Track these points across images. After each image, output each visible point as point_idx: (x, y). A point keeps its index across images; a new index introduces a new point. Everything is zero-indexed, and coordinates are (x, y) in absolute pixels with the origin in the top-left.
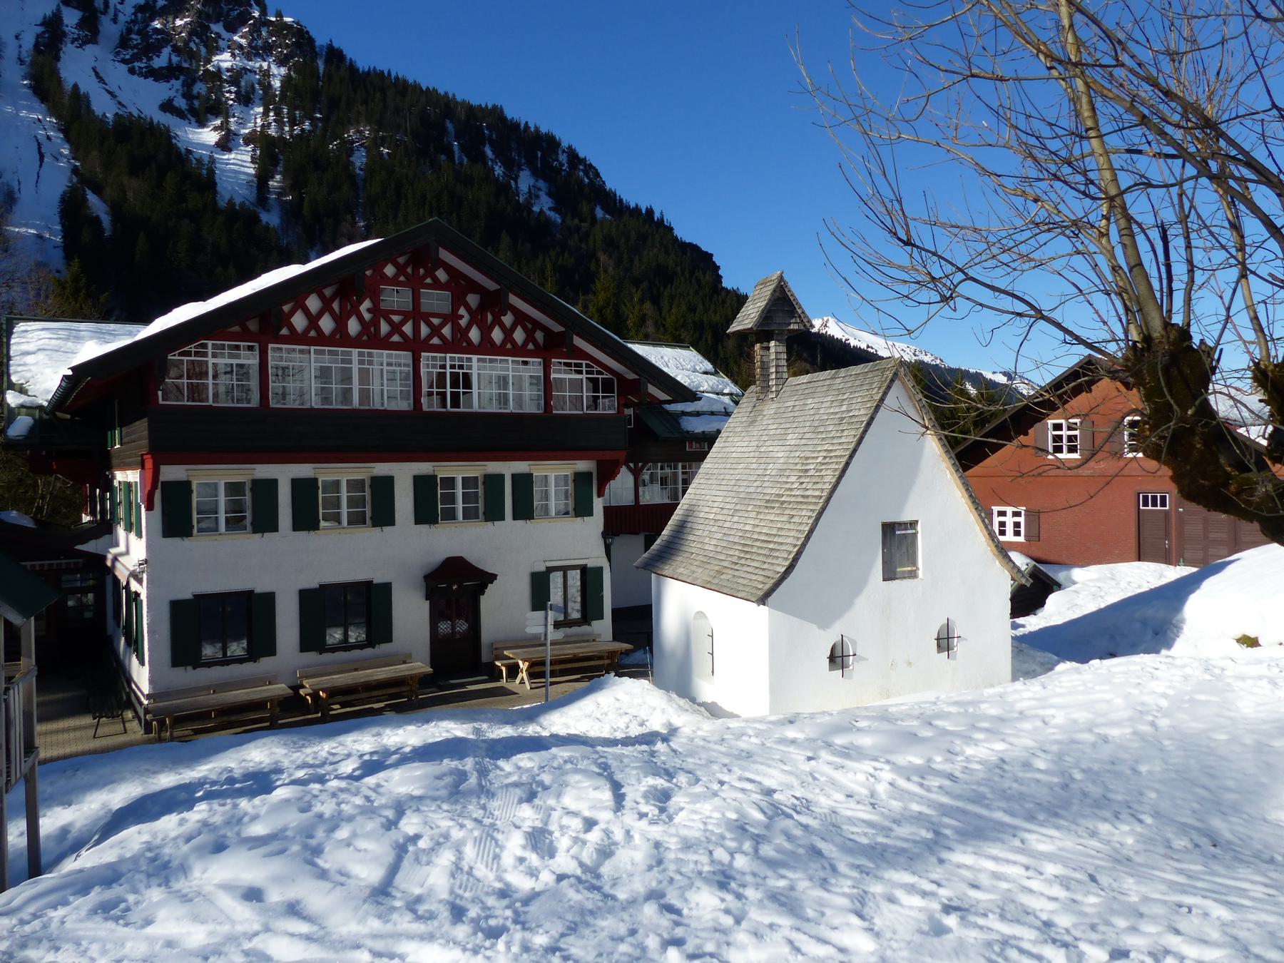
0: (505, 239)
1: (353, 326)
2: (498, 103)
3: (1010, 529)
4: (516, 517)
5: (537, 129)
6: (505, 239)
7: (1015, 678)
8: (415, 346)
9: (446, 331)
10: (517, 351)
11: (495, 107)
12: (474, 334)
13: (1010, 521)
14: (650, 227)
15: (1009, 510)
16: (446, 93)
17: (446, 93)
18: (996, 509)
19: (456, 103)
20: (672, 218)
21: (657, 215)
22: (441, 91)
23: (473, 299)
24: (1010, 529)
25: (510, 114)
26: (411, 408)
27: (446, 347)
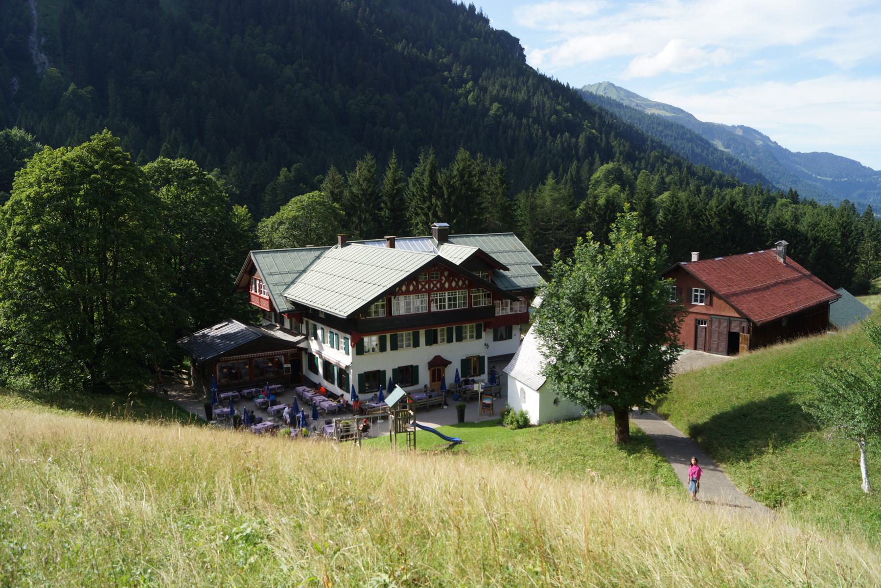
1: (411, 288)
4: (457, 341)
8: (429, 292)
9: (438, 285)
12: (447, 285)
21: (477, 11)
23: (446, 273)
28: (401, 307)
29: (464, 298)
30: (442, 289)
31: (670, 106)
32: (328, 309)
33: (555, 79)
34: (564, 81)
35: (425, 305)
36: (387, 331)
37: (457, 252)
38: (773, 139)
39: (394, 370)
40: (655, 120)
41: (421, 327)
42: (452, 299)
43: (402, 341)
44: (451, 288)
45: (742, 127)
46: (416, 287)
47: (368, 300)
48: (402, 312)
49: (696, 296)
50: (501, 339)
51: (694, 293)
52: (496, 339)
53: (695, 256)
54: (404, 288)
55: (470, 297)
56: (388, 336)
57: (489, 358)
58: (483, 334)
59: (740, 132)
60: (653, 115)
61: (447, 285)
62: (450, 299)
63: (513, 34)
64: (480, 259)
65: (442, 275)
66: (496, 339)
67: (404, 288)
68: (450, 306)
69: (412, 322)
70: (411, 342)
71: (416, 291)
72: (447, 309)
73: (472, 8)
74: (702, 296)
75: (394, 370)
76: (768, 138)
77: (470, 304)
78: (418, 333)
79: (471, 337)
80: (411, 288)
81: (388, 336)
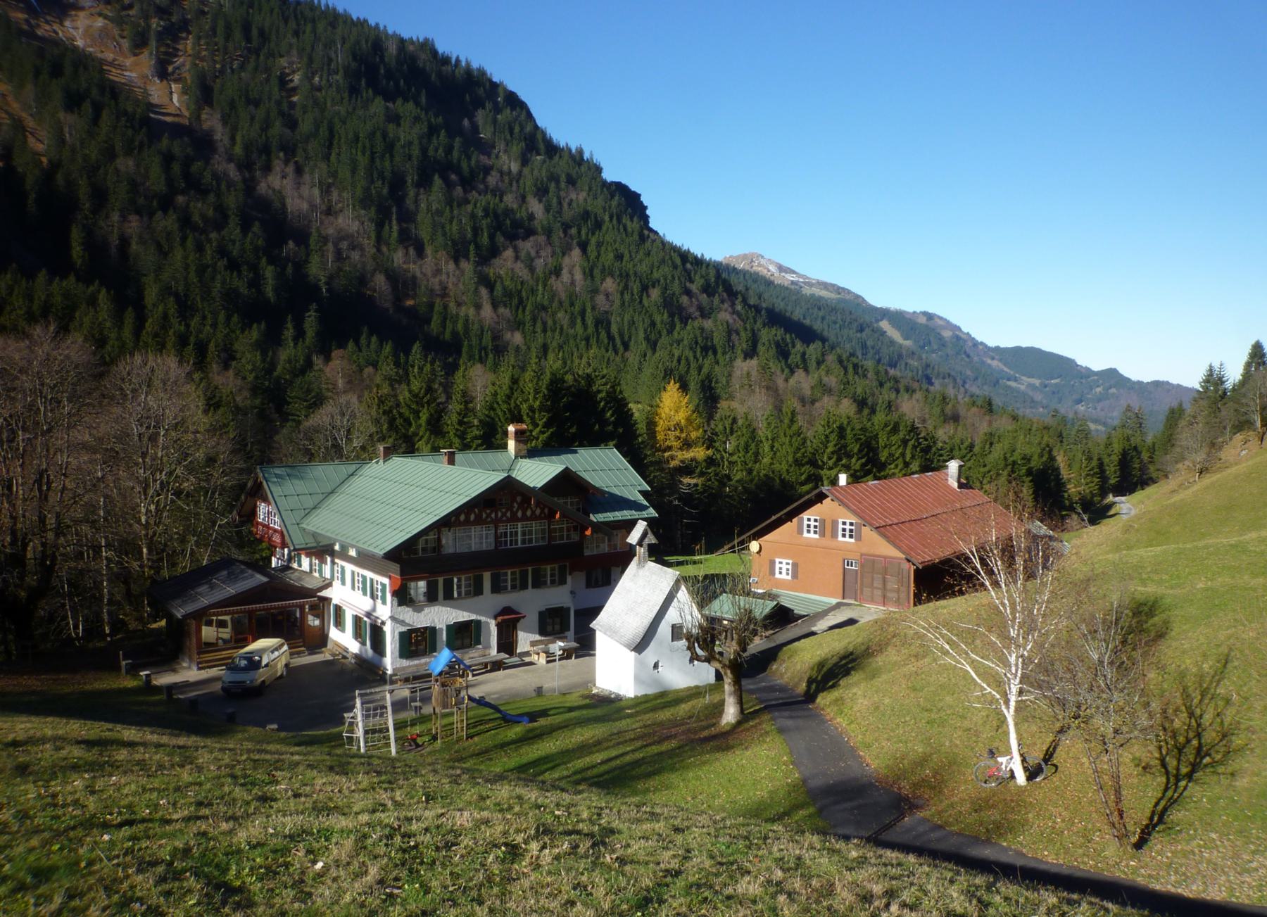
0: (438, 181)
1: (472, 517)
2: (430, 37)
3: (784, 571)
4: (533, 587)
5: (468, 64)
6: (438, 181)
7: (918, 600)
8: (496, 523)
9: (508, 514)
10: (539, 518)
11: (426, 40)
12: (520, 514)
13: (784, 567)
14: (580, 169)
15: (785, 561)
16: (377, 24)
17: (377, 24)
18: (777, 560)
19: (387, 34)
20: (600, 158)
21: (586, 156)
22: (372, 22)
23: (519, 499)
24: (784, 571)
25: (441, 48)
26: (493, 547)
27: (509, 520)
28: (451, 543)
29: (543, 531)
30: (514, 519)
31: (833, 285)
32: (371, 549)
33: (685, 248)
34: (1174, 380)
35: (492, 539)
36: (441, 573)
37: (537, 473)
38: (965, 330)
39: (448, 627)
40: (817, 304)
41: (486, 568)
42: (527, 532)
43: (506, 581)
44: (525, 518)
45: (925, 313)
46: (478, 518)
47: (414, 532)
48: (451, 551)
49: (844, 530)
50: (597, 585)
51: (841, 526)
52: (589, 585)
53: (843, 479)
54: (462, 518)
55: (550, 531)
56: (441, 580)
57: (576, 612)
58: (569, 579)
59: (923, 320)
60: (812, 295)
61: (520, 514)
62: (524, 534)
63: (633, 188)
64: (567, 482)
65: (514, 500)
66: (589, 585)
67: (462, 518)
68: (524, 542)
69: (472, 564)
70: (518, 582)
71: (479, 521)
72: (519, 545)
73: (580, 152)
74: (851, 531)
75: (448, 627)
76: (959, 329)
77: (550, 538)
78: (437, 582)
79: (514, 587)
80: (472, 517)
81: (441, 580)
